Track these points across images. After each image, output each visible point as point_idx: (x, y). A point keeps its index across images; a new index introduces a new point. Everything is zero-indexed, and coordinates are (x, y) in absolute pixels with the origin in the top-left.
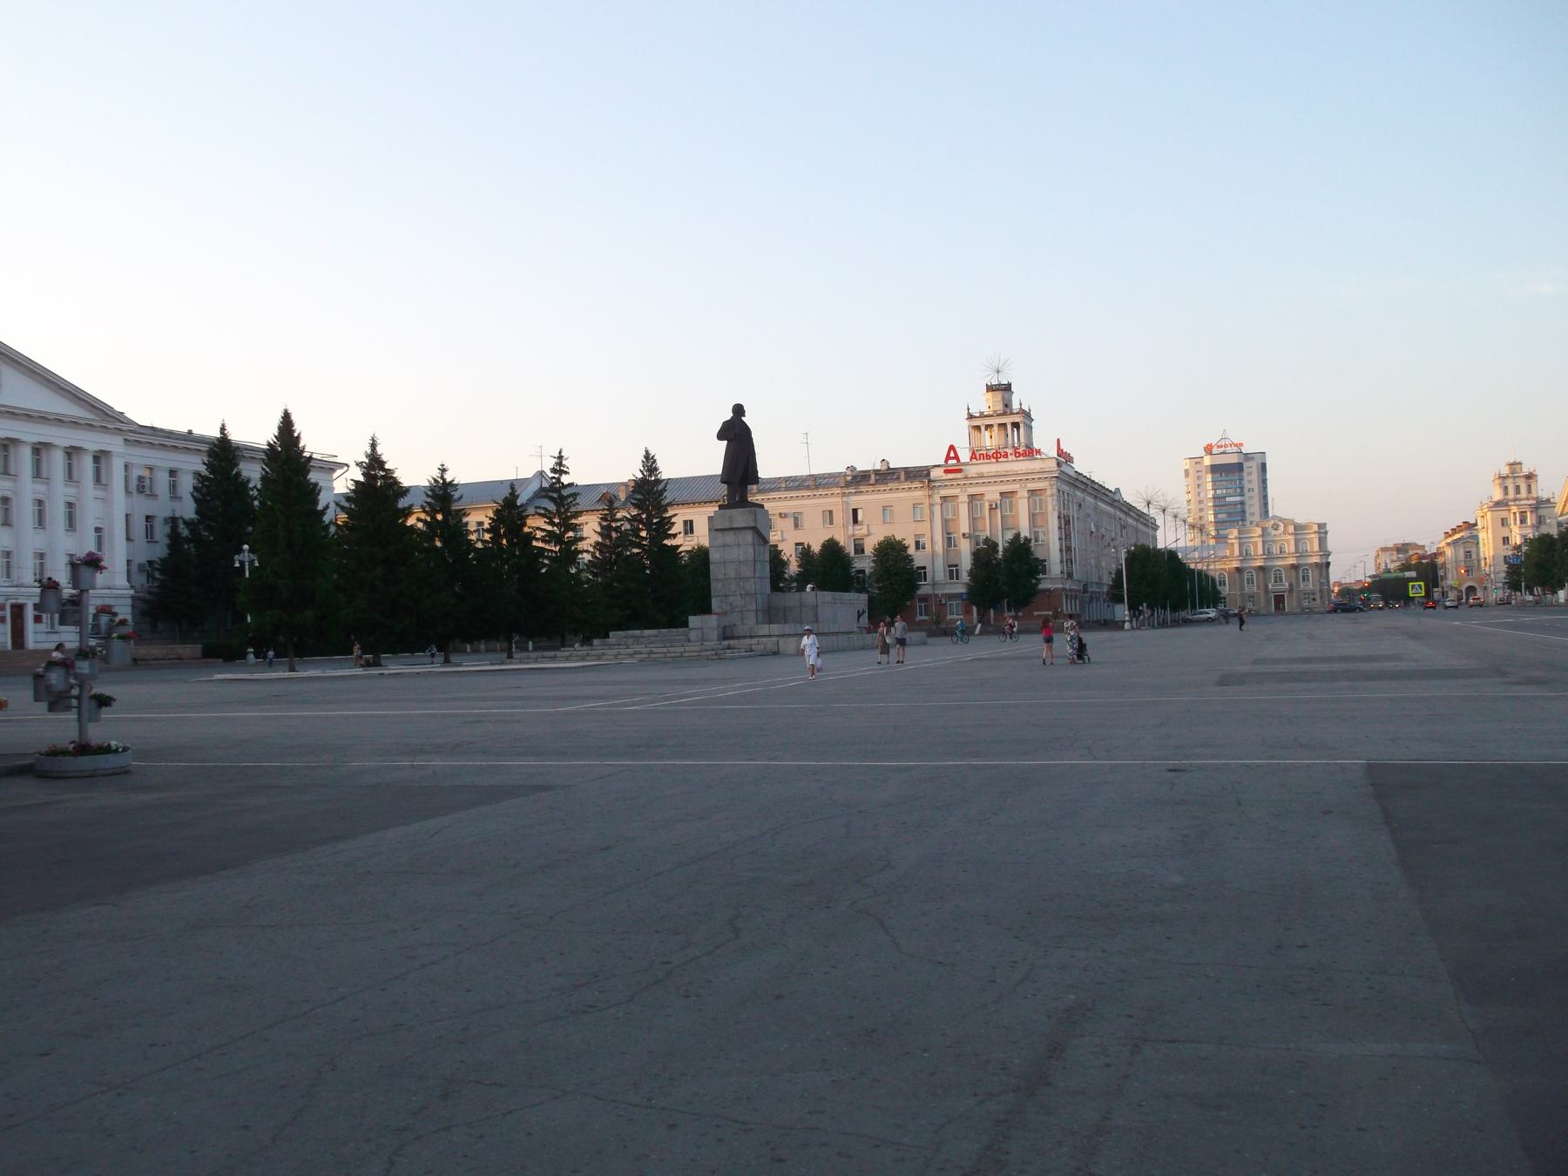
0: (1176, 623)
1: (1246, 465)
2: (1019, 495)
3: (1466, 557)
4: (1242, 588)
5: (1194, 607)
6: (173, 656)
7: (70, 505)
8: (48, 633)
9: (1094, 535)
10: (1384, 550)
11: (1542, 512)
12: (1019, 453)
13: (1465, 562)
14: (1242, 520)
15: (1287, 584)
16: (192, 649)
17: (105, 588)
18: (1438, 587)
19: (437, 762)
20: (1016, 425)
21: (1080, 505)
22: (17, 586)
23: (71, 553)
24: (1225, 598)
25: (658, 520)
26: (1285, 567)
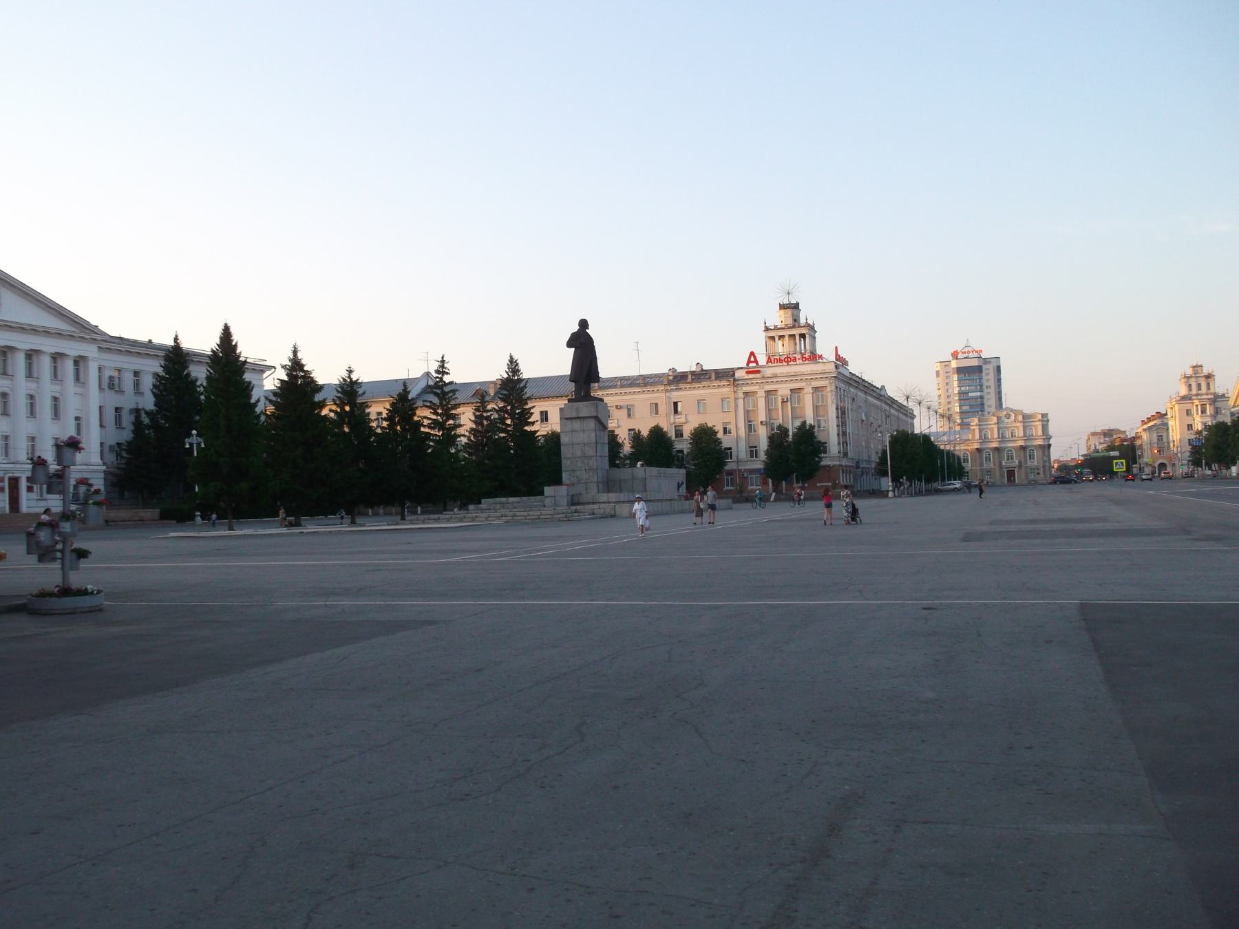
0: (929, 492)
1: (984, 367)
2: (805, 391)
3: (1158, 440)
4: (981, 465)
5: (943, 480)
6: (137, 518)
7: (55, 399)
8: (38, 500)
9: (864, 422)
10: (1094, 434)
11: (1218, 404)
12: (805, 358)
13: (1158, 444)
14: (981, 411)
15: (1017, 461)
16: (152, 513)
17: (83, 465)
18: (1136, 464)
19: (345, 602)
20: (803, 336)
21: (853, 399)
22: (13, 463)
23: (56, 437)
24: (968, 473)
25: (520, 411)
26: (1015, 448)
